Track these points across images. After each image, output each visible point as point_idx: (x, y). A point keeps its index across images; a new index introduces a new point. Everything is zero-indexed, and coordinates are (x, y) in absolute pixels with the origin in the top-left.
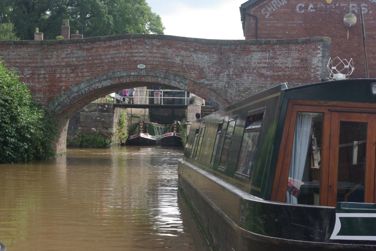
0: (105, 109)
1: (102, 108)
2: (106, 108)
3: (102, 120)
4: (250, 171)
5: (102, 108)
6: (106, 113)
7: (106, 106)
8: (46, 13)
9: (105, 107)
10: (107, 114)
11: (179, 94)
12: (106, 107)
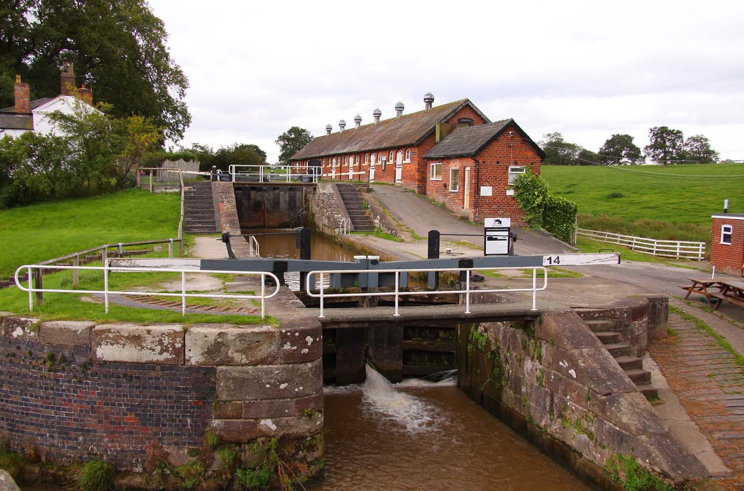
0: (306, 351)
3: (296, 390)
6: (309, 365)
7: (309, 339)
10: (310, 369)
12: (309, 344)
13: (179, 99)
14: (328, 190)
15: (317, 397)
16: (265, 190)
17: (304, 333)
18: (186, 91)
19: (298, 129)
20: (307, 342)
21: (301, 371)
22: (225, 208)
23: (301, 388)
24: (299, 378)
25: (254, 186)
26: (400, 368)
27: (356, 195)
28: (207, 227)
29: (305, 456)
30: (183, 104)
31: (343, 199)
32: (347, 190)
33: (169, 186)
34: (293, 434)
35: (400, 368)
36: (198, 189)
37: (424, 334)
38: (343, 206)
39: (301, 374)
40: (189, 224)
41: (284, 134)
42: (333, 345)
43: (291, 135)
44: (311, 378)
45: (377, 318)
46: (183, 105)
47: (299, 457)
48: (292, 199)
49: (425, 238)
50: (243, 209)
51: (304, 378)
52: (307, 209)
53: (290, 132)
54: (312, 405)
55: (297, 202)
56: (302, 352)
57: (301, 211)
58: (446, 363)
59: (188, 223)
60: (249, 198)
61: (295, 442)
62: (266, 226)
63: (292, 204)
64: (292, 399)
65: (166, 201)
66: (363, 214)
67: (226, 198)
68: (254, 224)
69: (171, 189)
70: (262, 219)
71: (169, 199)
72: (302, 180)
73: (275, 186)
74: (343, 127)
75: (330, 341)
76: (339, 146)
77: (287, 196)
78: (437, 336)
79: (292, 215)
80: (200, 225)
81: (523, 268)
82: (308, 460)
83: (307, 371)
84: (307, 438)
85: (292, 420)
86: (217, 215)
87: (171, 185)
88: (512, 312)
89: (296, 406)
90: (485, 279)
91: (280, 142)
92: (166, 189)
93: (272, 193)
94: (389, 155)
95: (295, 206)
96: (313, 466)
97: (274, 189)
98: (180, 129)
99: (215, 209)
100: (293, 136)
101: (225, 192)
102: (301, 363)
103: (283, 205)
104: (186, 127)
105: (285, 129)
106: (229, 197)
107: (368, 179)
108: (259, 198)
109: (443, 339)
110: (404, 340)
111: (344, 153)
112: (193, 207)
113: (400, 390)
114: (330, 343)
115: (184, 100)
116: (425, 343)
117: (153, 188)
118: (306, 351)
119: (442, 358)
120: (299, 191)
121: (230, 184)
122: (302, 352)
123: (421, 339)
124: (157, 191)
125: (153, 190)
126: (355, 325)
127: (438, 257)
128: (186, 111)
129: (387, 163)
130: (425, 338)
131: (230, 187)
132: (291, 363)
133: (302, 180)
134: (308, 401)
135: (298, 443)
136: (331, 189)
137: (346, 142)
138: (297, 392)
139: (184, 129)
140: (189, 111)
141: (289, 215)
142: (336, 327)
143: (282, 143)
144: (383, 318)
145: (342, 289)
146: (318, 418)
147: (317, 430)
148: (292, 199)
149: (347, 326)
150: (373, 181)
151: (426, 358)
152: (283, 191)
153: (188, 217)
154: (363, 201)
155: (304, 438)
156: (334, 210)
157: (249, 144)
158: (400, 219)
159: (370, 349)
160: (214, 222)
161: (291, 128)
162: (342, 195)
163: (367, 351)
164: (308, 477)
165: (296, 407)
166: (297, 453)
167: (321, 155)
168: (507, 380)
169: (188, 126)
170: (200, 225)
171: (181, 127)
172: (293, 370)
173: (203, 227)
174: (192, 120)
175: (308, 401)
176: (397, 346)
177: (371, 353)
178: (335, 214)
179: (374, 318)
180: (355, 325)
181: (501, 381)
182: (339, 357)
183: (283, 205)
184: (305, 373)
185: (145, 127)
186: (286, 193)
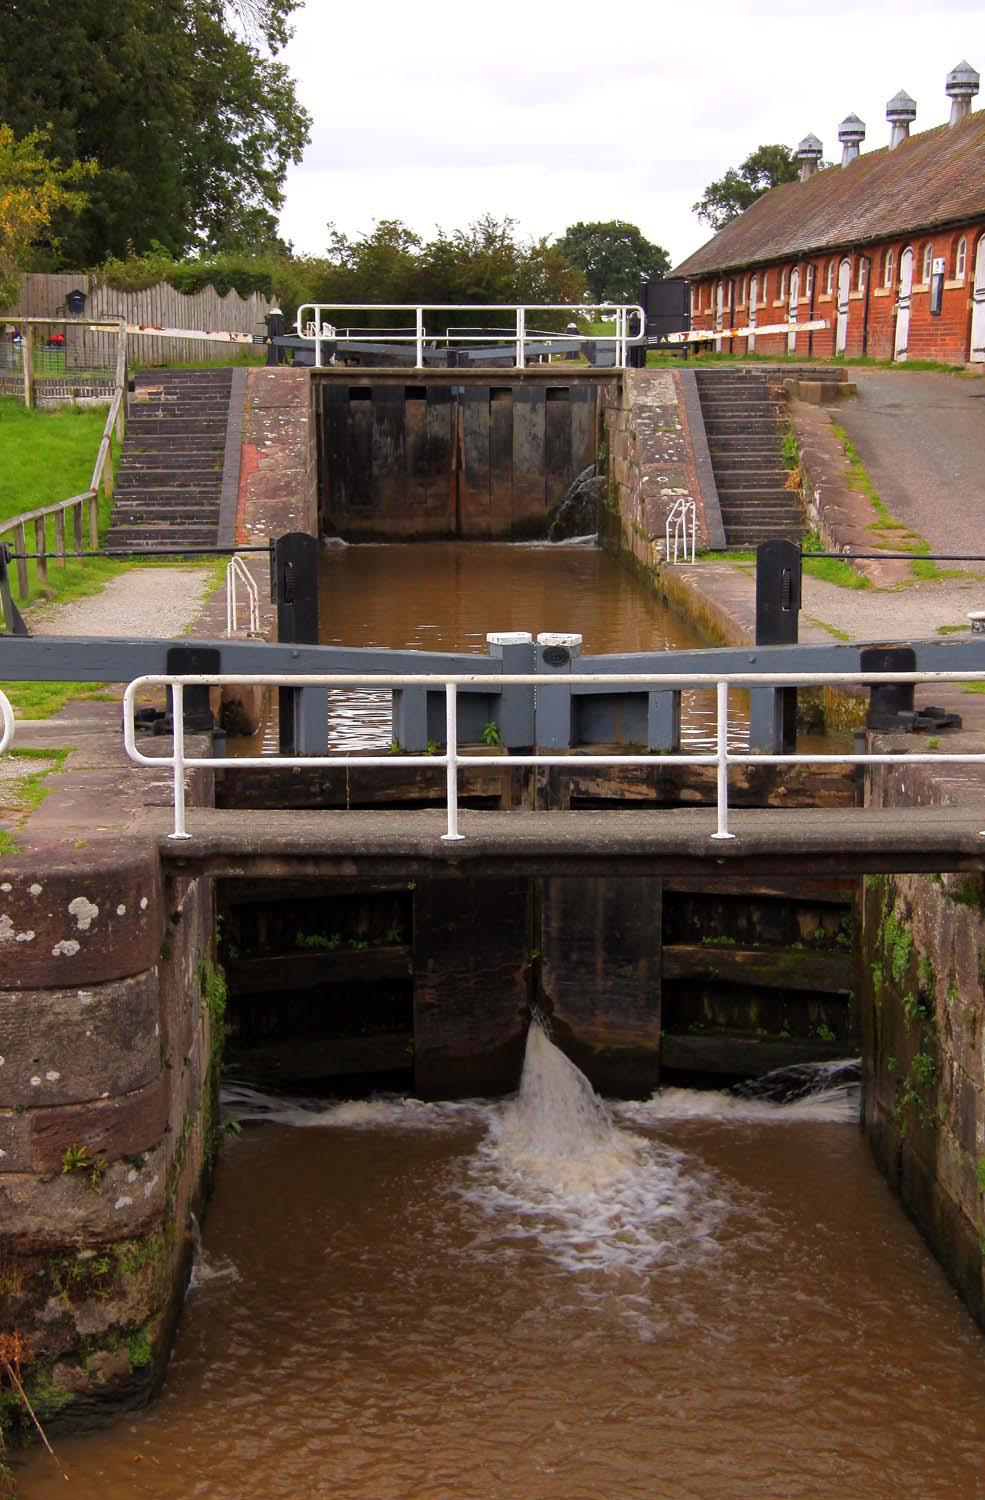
0: (71, 947)
1: (30, 935)
2: (81, 937)
3: (35, 1081)
4: (974, 1136)
5: (30, 935)
6: (85, 997)
7: (84, 910)
8: (801, 919)
9: (67, 926)
10: (90, 1010)
11: (492, 398)
12: (83, 924)
13: (265, 53)
14: (659, 396)
15: (116, 1111)
16: (462, 399)
17: (65, 887)
18: (291, 19)
19: (784, 157)
20: (74, 919)
21: (51, 1018)
22: (263, 463)
23: (53, 1076)
24: (41, 1042)
25: (418, 383)
26: (652, 1045)
27: (768, 411)
28: (185, 534)
29: (67, 1316)
30: (279, 71)
31: (710, 429)
32: (738, 393)
33: (84, 382)
34: (24, 1235)
35: (652, 1045)
36: (183, 397)
37: (743, 922)
38: (703, 456)
39: (51, 1027)
40: (125, 521)
41: (730, 175)
42: (400, 949)
43: (755, 180)
44: (90, 1041)
45: (382, 846)
46: (277, 77)
47: (47, 1319)
48: (559, 428)
49: (807, 573)
50: (375, 470)
51: (63, 1045)
52: (603, 468)
53: (753, 167)
54: (96, 1138)
55: (575, 444)
56: (56, 952)
57: (585, 480)
58: (824, 1032)
59: (124, 516)
60: (399, 430)
61: (33, 1264)
62: (465, 529)
63: (557, 455)
64: (20, 1110)
65: (64, 437)
66: (779, 482)
67: (276, 426)
68: (419, 524)
69: (94, 393)
70: (452, 506)
71: (75, 432)
72: (592, 359)
73: (555, 384)
74: (856, 144)
75: (393, 934)
76: (816, 223)
77: (540, 419)
78: (793, 934)
79: (557, 489)
80: (164, 526)
81: (944, 675)
82: (79, 1329)
83: (77, 1018)
84: (78, 1250)
85: (21, 1185)
86: (228, 490)
87: (93, 382)
88: (900, 841)
89: (36, 1136)
90: (964, 724)
91: (711, 208)
92: (77, 394)
93: (485, 407)
94: (954, 252)
95: (567, 457)
96: (100, 1354)
97: (494, 393)
98: (267, 167)
99: (229, 468)
100: (762, 184)
101: (279, 404)
102: (51, 989)
103: (526, 451)
104: (290, 163)
105: (731, 156)
106: (288, 423)
107: (888, 348)
108: (438, 429)
109: (811, 944)
110: (667, 941)
111: (819, 249)
112: (152, 462)
113: (619, 1121)
114: (394, 943)
115: (285, 56)
116: (740, 956)
117: (33, 391)
118: (71, 947)
119: (813, 1017)
120: (584, 399)
121: (302, 375)
122: (56, 952)
123: (732, 941)
124: (47, 402)
125: (34, 398)
126: (310, 870)
127: (794, 640)
128: (291, 100)
129: (948, 285)
130: (745, 938)
131: (297, 387)
132: (17, 989)
133: (592, 359)
134: (84, 1123)
135: (46, 1267)
136: (671, 392)
137: (842, 206)
138: (37, 1089)
139: (282, 167)
140: (301, 97)
141: (548, 490)
142: (240, 872)
143: (721, 213)
144: (400, 845)
145: (424, 744)
146: (123, 1182)
147: (118, 1226)
148: (559, 428)
149: (277, 870)
150: (903, 358)
151: (753, 1012)
152: (524, 401)
153: (126, 496)
154: (790, 436)
155: (67, 1251)
156: (661, 472)
157: (605, 220)
158: (902, 500)
159: (545, 970)
160: (216, 514)
161: (755, 151)
162: (707, 412)
163: (534, 978)
164: (76, 1391)
165: (34, 1142)
166: (42, 1304)
167: (757, 257)
168: (948, 1100)
169: (298, 159)
170: (164, 526)
171: (270, 161)
172: (23, 1013)
173: (171, 534)
174: (312, 133)
175: (84, 1123)
176: (643, 963)
177: (548, 986)
178: (664, 486)
179: (366, 845)
180: (310, 870)
181: (936, 1105)
182: (425, 996)
183: (526, 451)
184: (67, 1023)
185: (17, 166)
186: (534, 410)
